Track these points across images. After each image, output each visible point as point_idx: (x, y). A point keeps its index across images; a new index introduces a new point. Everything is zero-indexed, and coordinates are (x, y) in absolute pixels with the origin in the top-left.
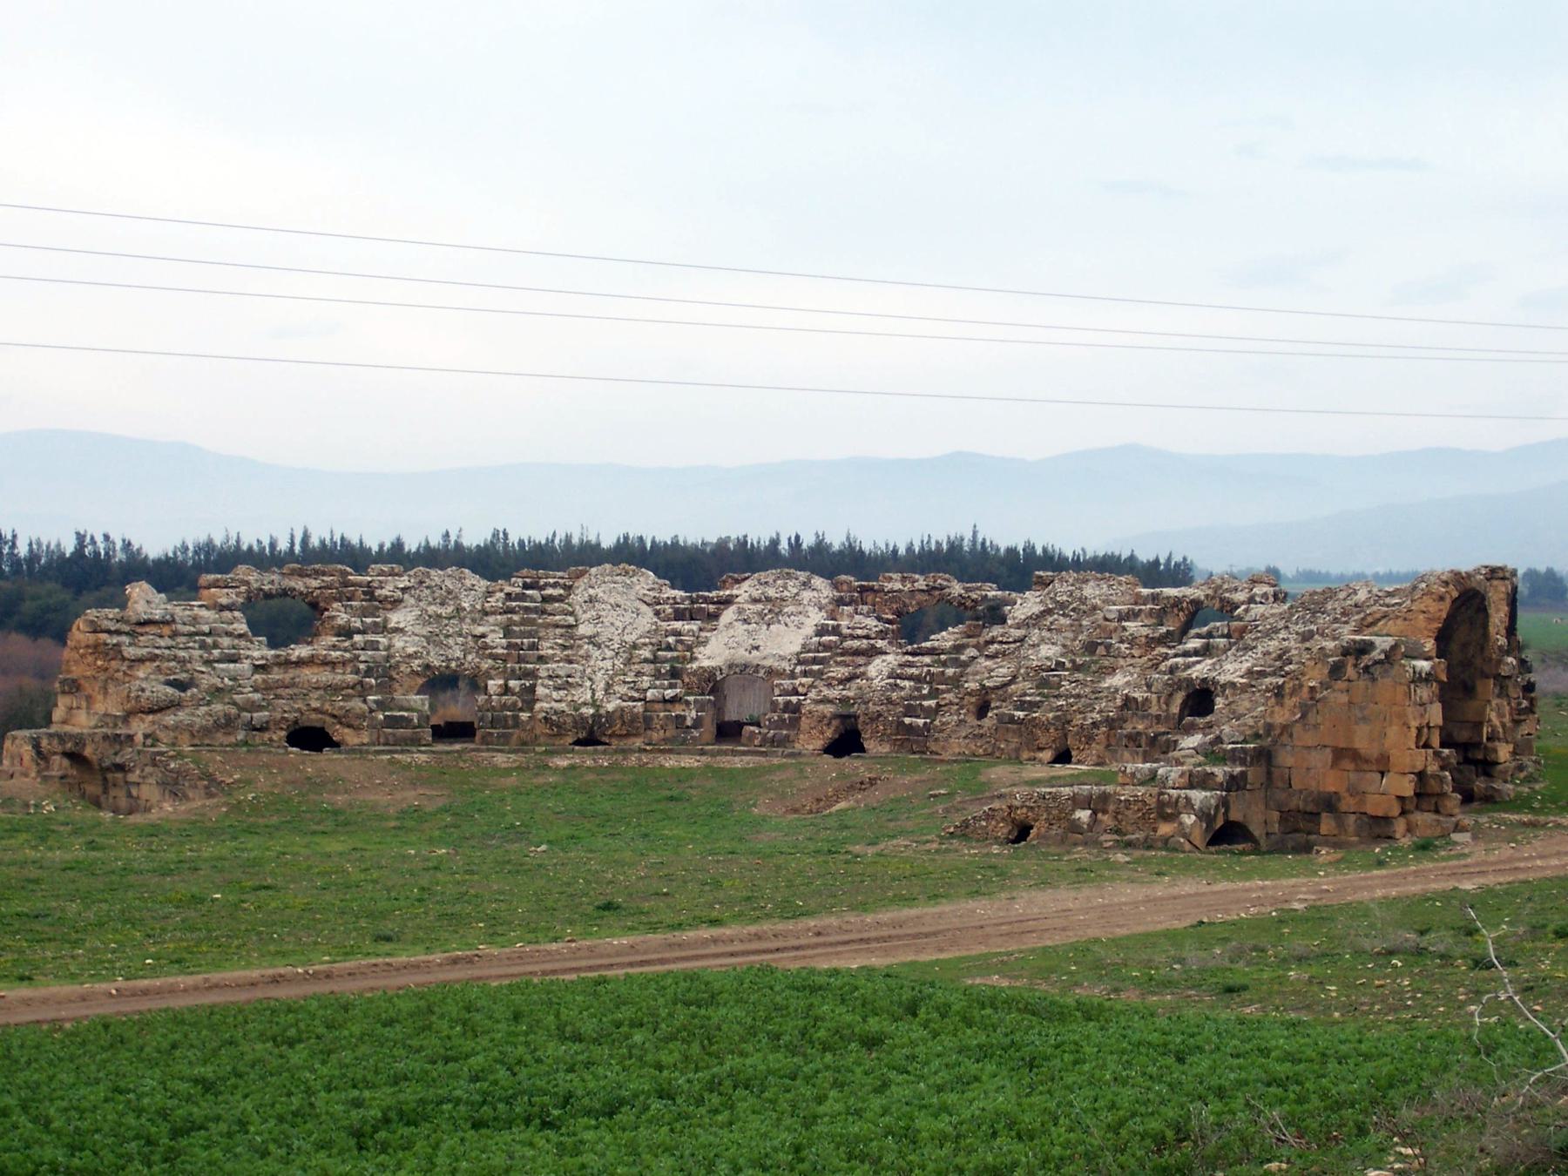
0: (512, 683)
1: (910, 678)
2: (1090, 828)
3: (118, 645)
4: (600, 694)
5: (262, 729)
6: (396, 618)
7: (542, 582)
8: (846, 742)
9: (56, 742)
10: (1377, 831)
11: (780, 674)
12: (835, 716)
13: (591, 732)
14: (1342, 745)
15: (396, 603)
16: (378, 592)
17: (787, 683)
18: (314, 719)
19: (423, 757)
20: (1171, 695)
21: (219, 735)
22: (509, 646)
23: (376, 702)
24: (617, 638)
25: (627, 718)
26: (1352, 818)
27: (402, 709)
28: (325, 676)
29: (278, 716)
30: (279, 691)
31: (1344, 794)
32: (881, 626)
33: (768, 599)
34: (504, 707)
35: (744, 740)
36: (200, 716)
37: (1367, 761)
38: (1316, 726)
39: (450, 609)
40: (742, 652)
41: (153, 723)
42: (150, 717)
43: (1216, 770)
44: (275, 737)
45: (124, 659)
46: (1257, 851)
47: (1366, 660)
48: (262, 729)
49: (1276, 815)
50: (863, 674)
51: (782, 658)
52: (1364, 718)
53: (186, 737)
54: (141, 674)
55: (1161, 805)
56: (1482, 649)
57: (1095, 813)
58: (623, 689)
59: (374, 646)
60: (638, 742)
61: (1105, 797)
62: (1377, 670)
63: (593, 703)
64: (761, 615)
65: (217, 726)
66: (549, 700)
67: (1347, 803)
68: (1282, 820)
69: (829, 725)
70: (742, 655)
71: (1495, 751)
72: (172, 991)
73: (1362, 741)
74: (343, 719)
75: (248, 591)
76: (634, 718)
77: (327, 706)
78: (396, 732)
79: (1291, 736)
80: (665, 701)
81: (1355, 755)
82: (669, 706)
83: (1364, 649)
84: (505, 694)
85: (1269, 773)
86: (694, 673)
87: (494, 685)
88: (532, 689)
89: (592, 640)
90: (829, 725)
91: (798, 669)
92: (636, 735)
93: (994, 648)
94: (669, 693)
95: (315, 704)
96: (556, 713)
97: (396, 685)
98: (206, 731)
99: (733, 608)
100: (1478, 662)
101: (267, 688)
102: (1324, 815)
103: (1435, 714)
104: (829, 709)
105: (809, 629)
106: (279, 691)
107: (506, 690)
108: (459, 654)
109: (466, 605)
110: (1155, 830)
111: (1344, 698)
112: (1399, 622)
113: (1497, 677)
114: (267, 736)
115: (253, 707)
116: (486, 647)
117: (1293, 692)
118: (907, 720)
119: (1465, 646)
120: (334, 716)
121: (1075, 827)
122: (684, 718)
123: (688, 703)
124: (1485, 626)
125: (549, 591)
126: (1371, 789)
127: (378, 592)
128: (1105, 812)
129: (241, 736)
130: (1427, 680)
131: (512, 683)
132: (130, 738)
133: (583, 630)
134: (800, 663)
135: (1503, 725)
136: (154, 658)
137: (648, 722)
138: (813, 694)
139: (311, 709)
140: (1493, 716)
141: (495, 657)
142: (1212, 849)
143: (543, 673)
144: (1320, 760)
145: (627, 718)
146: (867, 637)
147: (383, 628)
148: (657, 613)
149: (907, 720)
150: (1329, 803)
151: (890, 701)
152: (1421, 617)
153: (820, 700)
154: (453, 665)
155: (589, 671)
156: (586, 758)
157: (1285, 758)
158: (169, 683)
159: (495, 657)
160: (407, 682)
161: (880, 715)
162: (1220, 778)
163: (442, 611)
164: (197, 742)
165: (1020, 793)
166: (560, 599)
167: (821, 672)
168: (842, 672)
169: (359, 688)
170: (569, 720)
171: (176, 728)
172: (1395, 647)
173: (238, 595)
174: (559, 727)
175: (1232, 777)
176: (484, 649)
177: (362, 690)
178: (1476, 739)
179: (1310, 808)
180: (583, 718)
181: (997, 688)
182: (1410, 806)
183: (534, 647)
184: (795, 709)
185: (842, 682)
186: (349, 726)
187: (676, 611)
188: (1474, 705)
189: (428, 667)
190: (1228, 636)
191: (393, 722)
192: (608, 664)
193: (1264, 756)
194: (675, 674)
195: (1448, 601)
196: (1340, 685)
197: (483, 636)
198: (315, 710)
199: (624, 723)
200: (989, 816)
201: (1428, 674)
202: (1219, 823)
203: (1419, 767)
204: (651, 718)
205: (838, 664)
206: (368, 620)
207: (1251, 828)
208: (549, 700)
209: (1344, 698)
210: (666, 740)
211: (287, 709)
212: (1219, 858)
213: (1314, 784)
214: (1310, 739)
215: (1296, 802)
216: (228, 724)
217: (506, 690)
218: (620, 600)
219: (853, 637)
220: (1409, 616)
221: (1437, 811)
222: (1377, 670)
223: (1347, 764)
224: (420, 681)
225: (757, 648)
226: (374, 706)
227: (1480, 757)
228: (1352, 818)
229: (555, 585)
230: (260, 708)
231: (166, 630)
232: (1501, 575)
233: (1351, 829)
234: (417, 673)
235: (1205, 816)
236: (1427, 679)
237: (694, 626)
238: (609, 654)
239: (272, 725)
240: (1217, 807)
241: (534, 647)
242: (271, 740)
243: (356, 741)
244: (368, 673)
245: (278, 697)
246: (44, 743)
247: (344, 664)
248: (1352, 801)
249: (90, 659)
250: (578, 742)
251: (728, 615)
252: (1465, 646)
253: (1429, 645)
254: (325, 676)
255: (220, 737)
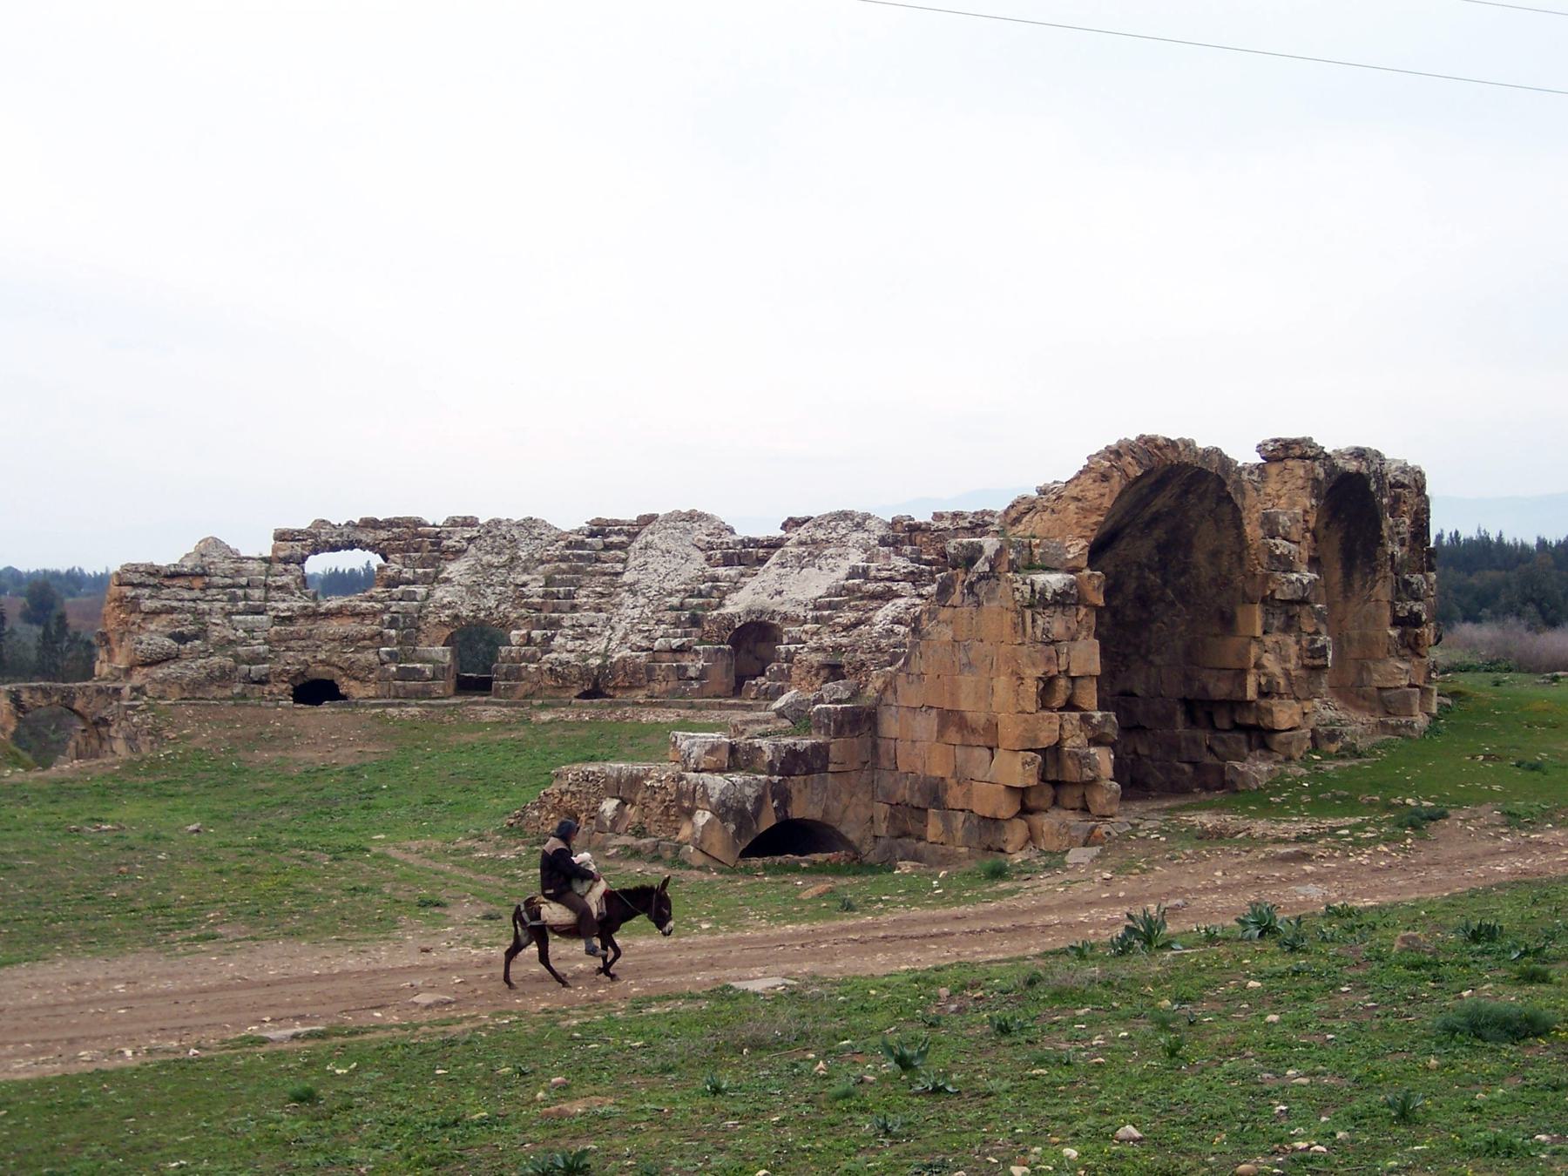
0: (534, 633)
3: (136, 597)
5: (262, 682)
9: (39, 695)
13: (596, 684)
14: (947, 707)
15: (458, 553)
18: (320, 672)
19: (414, 711)
21: (214, 688)
22: (546, 595)
23: (388, 653)
24: (656, 586)
25: (629, 668)
26: (961, 816)
28: (350, 627)
29: (279, 668)
30: (292, 644)
31: (951, 782)
32: (912, 567)
33: (814, 542)
34: (524, 658)
36: (192, 668)
37: (974, 731)
38: (921, 675)
39: (505, 558)
40: (764, 597)
41: (147, 675)
42: (145, 670)
44: (275, 691)
46: (858, 865)
48: (262, 682)
49: (882, 810)
50: (869, 619)
51: (799, 603)
52: (970, 664)
53: (176, 690)
54: (152, 627)
56: (1241, 559)
57: (624, 803)
58: (635, 638)
59: (411, 596)
60: (640, 696)
61: (635, 781)
62: (982, 588)
64: (799, 558)
65: (211, 679)
66: (564, 649)
67: (955, 797)
68: (892, 818)
69: (817, 675)
71: (1270, 712)
74: (349, 671)
76: (637, 669)
77: (335, 659)
78: (408, 684)
79: (895, 692)
82: (678, 656)
84: (528, 644)
85: (875, 746)
86: (714, 621)
87: (515, 636)
89: (632, 589)
90: (817, 675)
92: (641, 687)
94: (676, 642)
96: (561, 664)
97: (422, 636)
98: (196, 684)
99: (779, 552)
100: (1238, 579)
102: (931, 811)
103: (1086, 656)
104: (819, 658)
105: (842, 573)
106: (292, 644)
107: (529, 640)
108: (493, 604)
109: (523, 554)
112: (1046, 516)
113: (1268, 601)
114: (267, 688)
115: (256, 659)
116: (523, 596)
119: (1215, 555)
122: (686, 669)
123: (697, 653)
124: (1238, 524)
126: (979, 774)
129: (238, 689)
130: (1055, 603)
131: (534, 633)
132: (117, 691)
133: (628, 577)
134: (816, 608)
135: (1287, 673)
136: (172, 610)
137: (650, 671)
139: (319, 661)
140: (1270, 661)
141: (528, 606)
142: (756, 862)
143: (567, 623)
145: (629, 668)
146: (891, 579)
150: (934, 794)
151: (879, 649)
152: (1072, 507)
154: (482, 614)
155: (616, 619)
156: (587, 712)
157: (890, 725)
158: (171, 636)
159: (528, 606)
160: (434, 633)
161: (863, 665)
163: (495, 560)
164: (186, 695)
165: (98, 774)
167: (830, 618)
169: (378, 639)
170: (575, 672)
171: (163, 681)
174: (564, 679)
175: (793, 753)
176: (520, 598)
178: (1238, 695)
179: (917, 801)
180: (588, 669)
182: (1032, 802)
183: (569, 595)
185: (847, 628)
186: (356, 679)
187: (725, 556)
188: (1234, 643)
189: (456, 617)
191: (405, 675)
192: (637, 612)
194: (695, 621)
195: (1117, 483)
196: (945, 614)
198: (321, 661)
199: (626, 674)
201: (1065, 594)
202: (768, 821)
203: (1046, 739)
204: (654, 669)
205: (851, 608)
206: (420, 571)
207: (843, 829)
209: (948, 633)
211: (291, 660)
212: (764, 881)
213: (919, 765)
215: (903, 793)
216: (223, 677)
217: (529, 640)
218: (672, 545)
220: (1059, 506)
221: (1085, 809)
222: (982, 588)
223: (953, 736)
224: (447, 632)
225: (780, 593)
226: (385, 658)
227: (1251, 721)
228: (961, 816)
230: (265, 660)
231: (198, 583)
232: (1298, 452)
233: (959, 834)
234: (444, 624)
235: (726, 810)
236: (1062, 600)
237: (733, 572)
238: (642, 601)
239: (272, 678)
240: (760, 800)
241: (569, 595)
242: (271, 693)
243: (363, 694)
245: (288, 649)
246: (25, 696)
250: (585, 695)
252: (1215, 555)
253: (1076, 549)
254: (350, 627)
255: (215, 691)
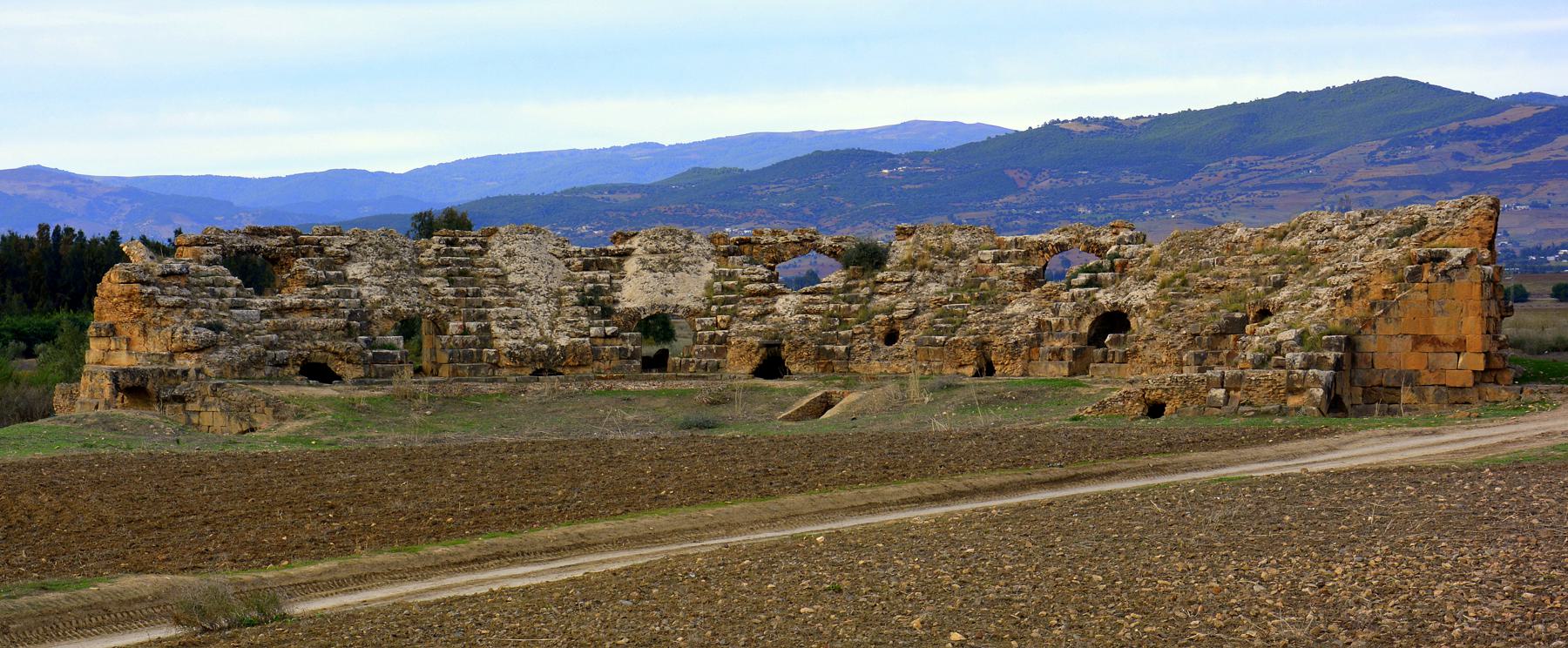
1: (818, 312)
2: (1226, 403)
3: (152, 294)
4: (547, 332)
6: (353, 270)
7: (462, 240)
8: (772, 365)
10: (1456, 398)
11: (696, 313)
12: (762, 345)
16: (328, 250)
17: (708, 321)
20: (1080, 318)
22: (456, 294)
26: (1432, 389)
27: (384, 347)
33: (663, 252)
35: (669, 368)
43: (1327, 354)
45: (159, 306)
47: (1441, 267)
55: (1290, 381)
57: (1228, 391)
63: (545, 341)
66: (504, 340)
70: (658, 297)
72: (552, 571)
73: (1440, 329)
75: (223, 249)
80: (606, 337)
81: (1435, 341)
83: (1438, 258)
86: (621, 314)
87: (454, 326)
88: (487, 329)
91: (714, 308)
93: (887, 287)
94: (609, 330)
95: (320, 343)
101: (277, 330)
104: (757, 340)
107: (465, 331)
110: (1285, 402)
111: (1425, 296)
115: (271, 346)
117: (1362, 294)
118: (828, 347)
120: (335, 353)
121: (1213, 403)
125: (470, 247)
127: (328, 250)
128: (1236, 390)
133: (512, 279)
138: (734, 328)
144: (1402, 346)
147: (343, 278)
148: (568, 265)
149: (828, 347)
150: (1411, 379)
153: (747, 332)
162: (1332, 361)
166: (481, 254)
168: (753, 310)
172: (1470, 256)
173: (215, 251)
177: (349, 332)
181: (905, 318)
183: (477, 294)
184: (724, 340)
186: (349, 362)
189: (395, 310)
190: (1112, 269)
193: (1351, 344)
197: (432, 285)
200: (1125, 397)
206: (332, 273)
208: (504, 340)
210: (613, 369)
213: (1395, 364)
214: (1392, 329)
219: (751, 281)
223: (1426, 347)
228: (1432, 389)
229: (473, 243)
231: (182, 281)
241: (477, 294)
244: (352, 316)
247: (327, 310)
248: (1431, 376)
249: (125, 307)
251: (631, 265)
